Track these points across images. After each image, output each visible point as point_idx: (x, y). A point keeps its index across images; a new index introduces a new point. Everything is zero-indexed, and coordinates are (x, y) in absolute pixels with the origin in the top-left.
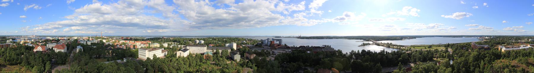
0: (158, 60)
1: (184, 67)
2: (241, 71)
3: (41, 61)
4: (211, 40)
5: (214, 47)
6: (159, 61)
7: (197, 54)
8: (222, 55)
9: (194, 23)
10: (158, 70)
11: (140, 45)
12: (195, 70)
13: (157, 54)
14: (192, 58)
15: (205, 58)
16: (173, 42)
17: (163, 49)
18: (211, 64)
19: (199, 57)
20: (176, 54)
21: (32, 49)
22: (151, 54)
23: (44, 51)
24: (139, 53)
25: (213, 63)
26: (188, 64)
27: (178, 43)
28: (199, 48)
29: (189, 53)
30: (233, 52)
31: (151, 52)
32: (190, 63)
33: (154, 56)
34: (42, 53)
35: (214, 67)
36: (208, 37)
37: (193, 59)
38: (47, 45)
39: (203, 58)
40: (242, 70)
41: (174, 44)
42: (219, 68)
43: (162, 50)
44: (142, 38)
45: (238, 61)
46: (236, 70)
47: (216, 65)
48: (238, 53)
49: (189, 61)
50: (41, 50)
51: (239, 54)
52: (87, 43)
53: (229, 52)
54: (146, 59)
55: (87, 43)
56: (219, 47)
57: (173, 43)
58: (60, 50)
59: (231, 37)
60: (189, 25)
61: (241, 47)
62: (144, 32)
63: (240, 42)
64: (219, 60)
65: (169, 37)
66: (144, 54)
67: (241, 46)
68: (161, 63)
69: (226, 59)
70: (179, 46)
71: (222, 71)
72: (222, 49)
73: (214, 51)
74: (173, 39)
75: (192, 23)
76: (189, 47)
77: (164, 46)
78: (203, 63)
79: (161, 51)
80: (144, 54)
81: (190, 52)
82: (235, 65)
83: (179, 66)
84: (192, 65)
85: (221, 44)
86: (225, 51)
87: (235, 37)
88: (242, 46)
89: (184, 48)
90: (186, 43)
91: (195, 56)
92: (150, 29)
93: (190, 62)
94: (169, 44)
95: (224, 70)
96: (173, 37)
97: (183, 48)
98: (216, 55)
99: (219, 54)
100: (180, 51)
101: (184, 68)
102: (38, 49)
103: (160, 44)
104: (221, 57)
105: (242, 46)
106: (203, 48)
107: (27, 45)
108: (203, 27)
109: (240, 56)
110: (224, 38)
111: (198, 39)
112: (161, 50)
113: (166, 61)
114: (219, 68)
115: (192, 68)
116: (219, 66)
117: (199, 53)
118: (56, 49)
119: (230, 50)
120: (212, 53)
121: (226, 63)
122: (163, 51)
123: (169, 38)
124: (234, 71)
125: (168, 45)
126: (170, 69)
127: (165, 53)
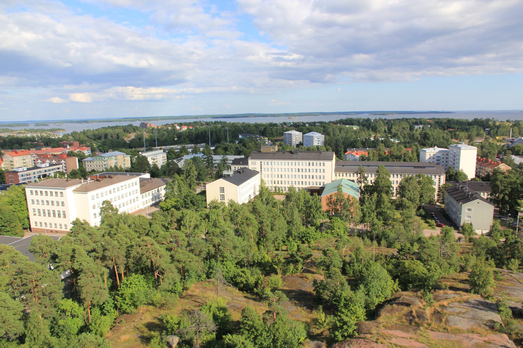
0: (122, 225)
1: (238, 244)
2: (492, 281)
4: (355, 132)
5: (366, 163)
6: (128, 230)
7: (290, 189)
8: (403, 196)
9: (295, 56)
10: (127, 267)
11: (36, 167)
12: (282, 256)
13: (121, 201)
14: (270, 207)
15: (325, 207)
16: (191, 142)
17: (147, 176)
18: (351, 233)
19: (302, 203)
20: (204, 193)
22: (91, 203)
24: (31, 206)
25: (359, 230)
26: (252, 231)
27: (212, 145)
28: (303, 164)
29: (258, 188)
30: (455, 189)
31: (90, 194)
32: (261, 230)
33: (103, 210)
35: (362, 247)
36: (344, 117)
37: (276, 210)
39: (318, 208)
40: (495, 279)
41: (195, 151)
42: (385, 250)
43: (142, 181)
44: (42, 131)
45: (479, 232)
46: (463, 269)
47: (372, 240)
48: (485, 195)
49: (255, 222)
51: (490, 201)
53: (436, 187)
54: (70, 226)
56: (390, 163)
57: (190, 147)
59: (450, 117)
60: (274, 63)
61: (503, 167)
62: (56, 100)
63: (499, 141)
64: (386, 220)
65: (170, 122)
66: (56, 208)
67: (502, 161)
68: (137, 235)
69: (420, 215)
70: (217, 158)
71: (397, 266)
72: (405, 172)
73: (366, 178)
74: (190, 131)
75: (285, 57)
76: (258, 162)
77: (151, 162)
78: (319, 228)
79: (138, 187)
80: (61, 208)
81: (262, 181)
82: (459, 249)
83: (217, 241)
84: (270, 235)
85: (399, 150)
86: (419, 183)
87: (470, 119)
88: (510, 163)
89: (238, 167)
90: (244, 145)
91: (282, 198)
92: (85, 85)
93: (261, 223)
94: (170, 155)
95: (407, 263)
96: (188, 121)
97: (233, 167)
98: (375, 194)
99: (387, 193)
100: (221, 182)
101: (235, 248)
103: (132, 155)
104: (399, 206)
105: (510, 163)
106: (318, 167)
108: (336, 70)
109: (490, 209)
110: (417, 124)
111: (298, 127)
112: (137, 180)
113: (157, 228)
114: (385, 250)
115: (272, 248)
116: (383, 242)
117: (301, 186)
119: (443, 178)
120: (356, 185)
121: (417, 233)
122: (144, 187)
123: (173, 125)
124: (452, 273)
125: (168, 158)
126: (176, 257)
127: (155, 191)
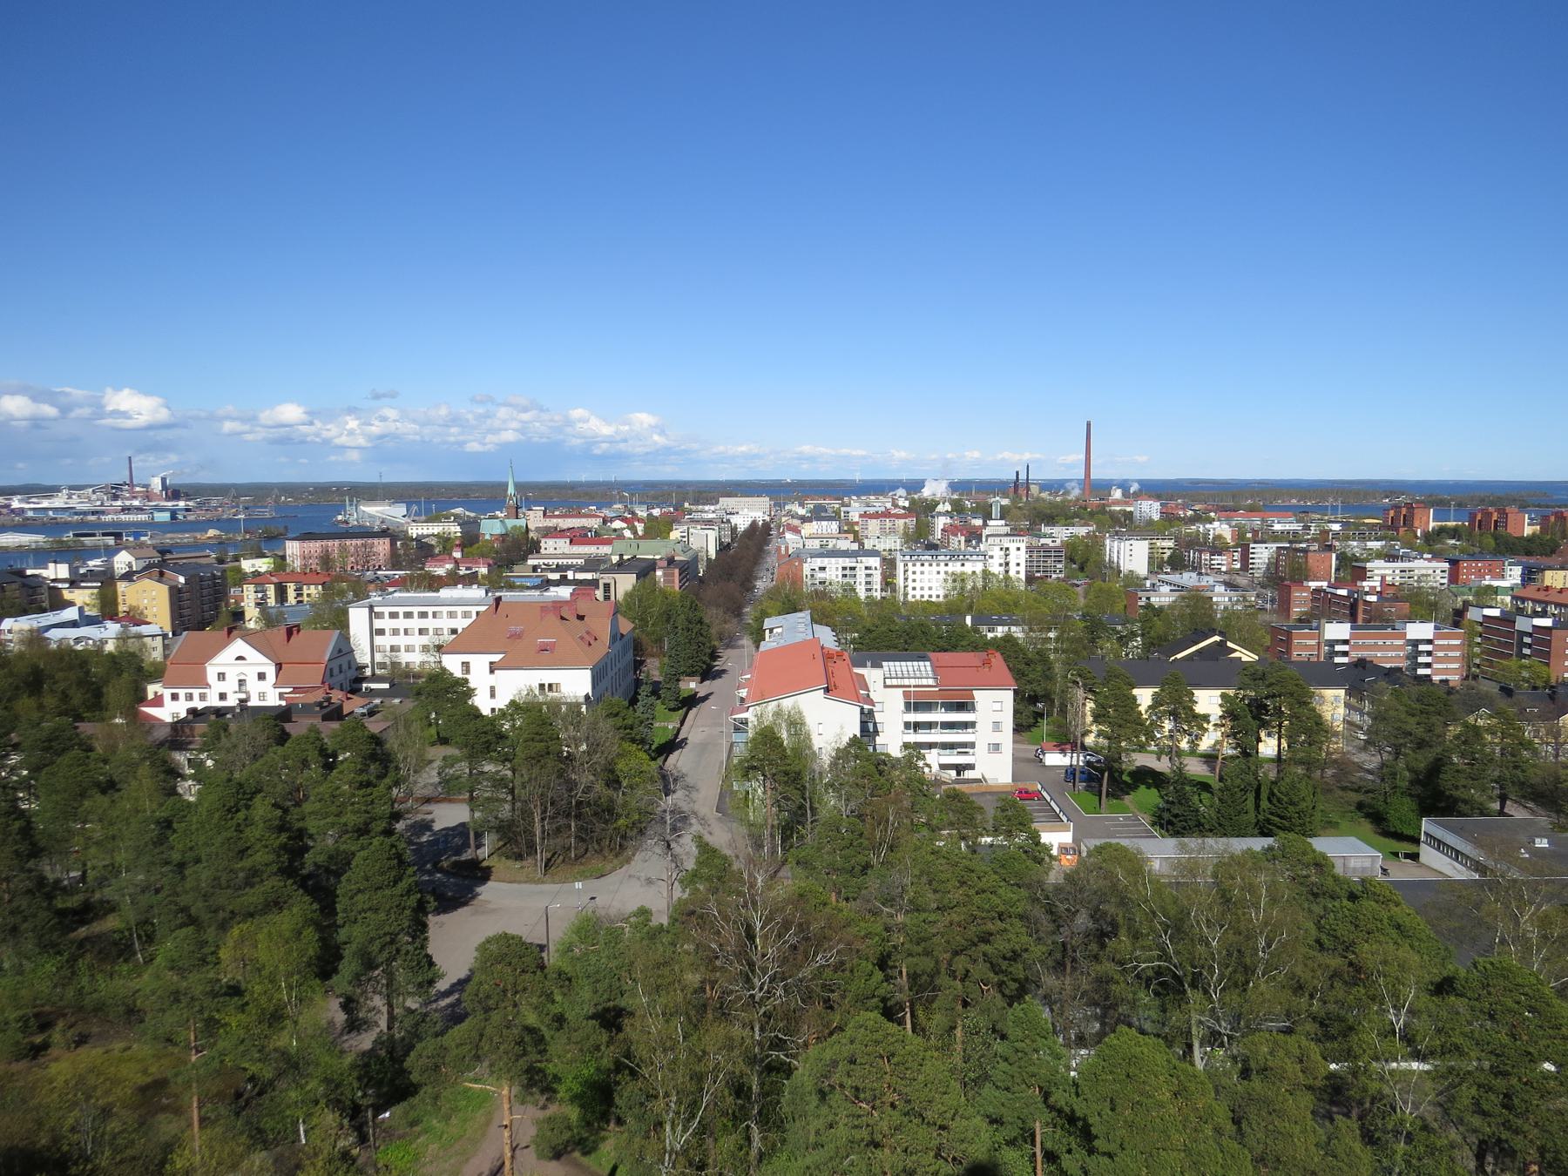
3: (260, 857)
21: (115, 693)
23: (307, 708)
34: (283, 738)
38: (358, 618)
50: (267, 694)
52: (888, 582)
55: (888, 582)
58: (548, 676)
102: (217, 687)
107: (36, 638)
118: (480, 663)
